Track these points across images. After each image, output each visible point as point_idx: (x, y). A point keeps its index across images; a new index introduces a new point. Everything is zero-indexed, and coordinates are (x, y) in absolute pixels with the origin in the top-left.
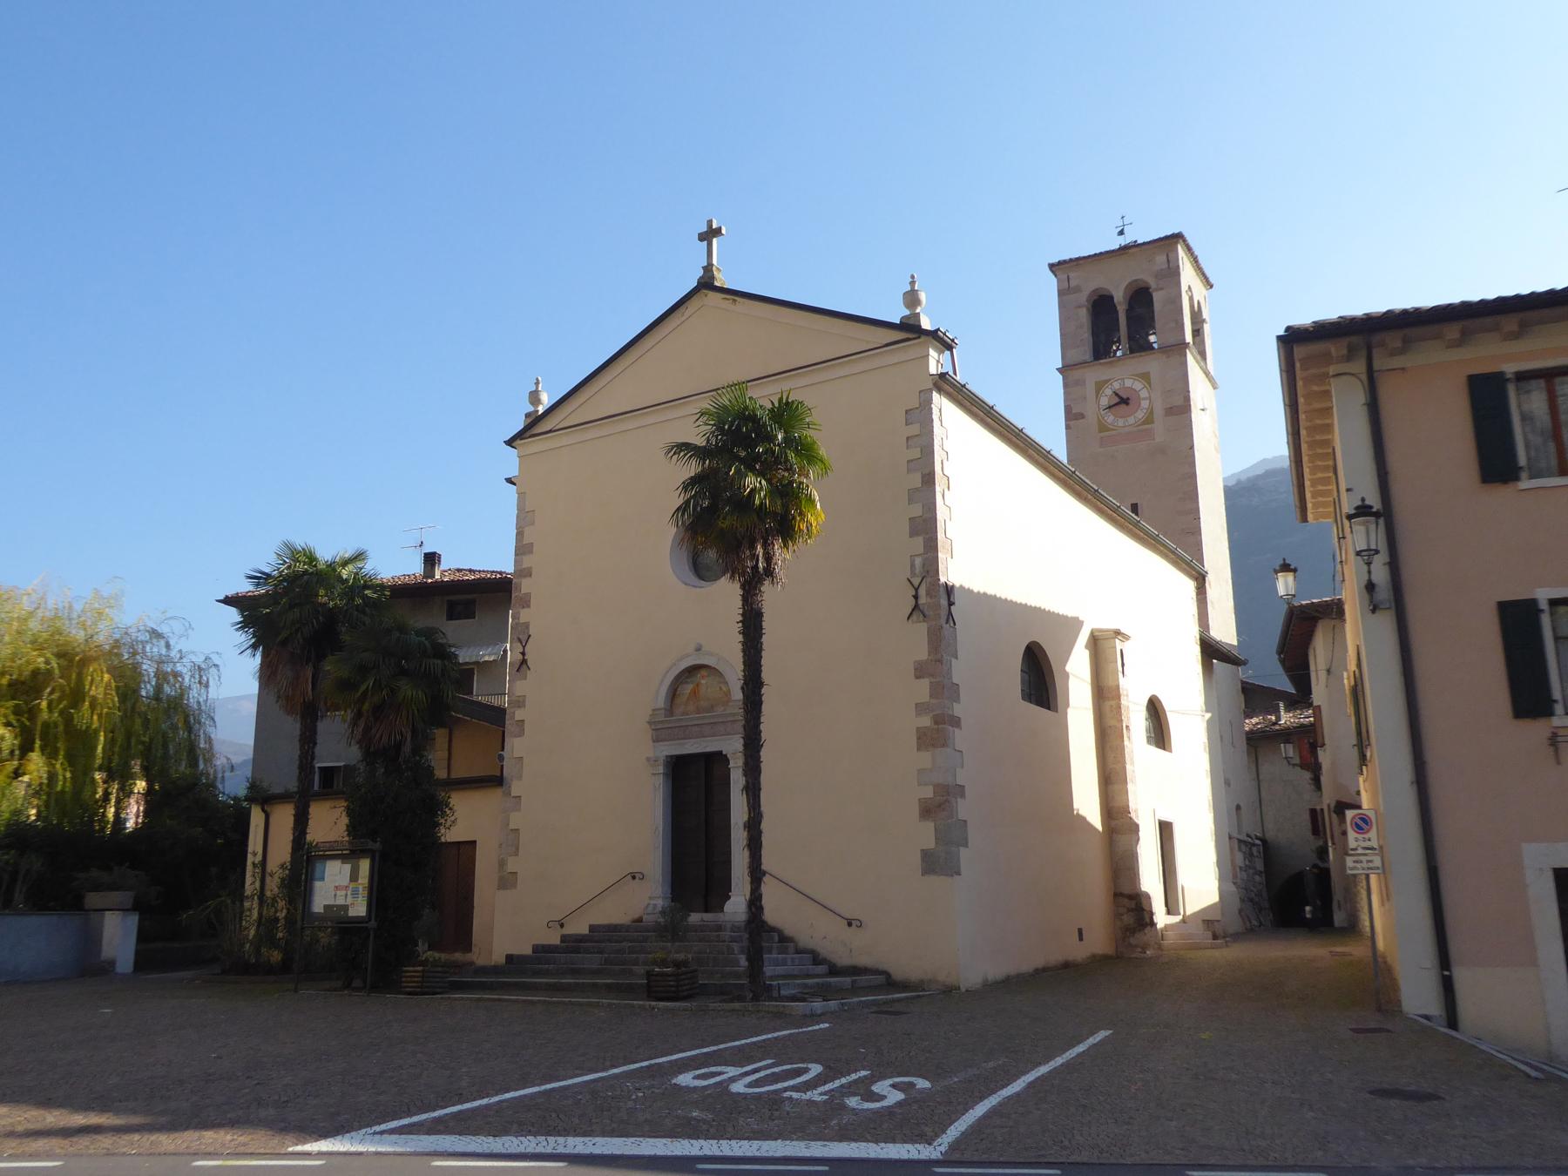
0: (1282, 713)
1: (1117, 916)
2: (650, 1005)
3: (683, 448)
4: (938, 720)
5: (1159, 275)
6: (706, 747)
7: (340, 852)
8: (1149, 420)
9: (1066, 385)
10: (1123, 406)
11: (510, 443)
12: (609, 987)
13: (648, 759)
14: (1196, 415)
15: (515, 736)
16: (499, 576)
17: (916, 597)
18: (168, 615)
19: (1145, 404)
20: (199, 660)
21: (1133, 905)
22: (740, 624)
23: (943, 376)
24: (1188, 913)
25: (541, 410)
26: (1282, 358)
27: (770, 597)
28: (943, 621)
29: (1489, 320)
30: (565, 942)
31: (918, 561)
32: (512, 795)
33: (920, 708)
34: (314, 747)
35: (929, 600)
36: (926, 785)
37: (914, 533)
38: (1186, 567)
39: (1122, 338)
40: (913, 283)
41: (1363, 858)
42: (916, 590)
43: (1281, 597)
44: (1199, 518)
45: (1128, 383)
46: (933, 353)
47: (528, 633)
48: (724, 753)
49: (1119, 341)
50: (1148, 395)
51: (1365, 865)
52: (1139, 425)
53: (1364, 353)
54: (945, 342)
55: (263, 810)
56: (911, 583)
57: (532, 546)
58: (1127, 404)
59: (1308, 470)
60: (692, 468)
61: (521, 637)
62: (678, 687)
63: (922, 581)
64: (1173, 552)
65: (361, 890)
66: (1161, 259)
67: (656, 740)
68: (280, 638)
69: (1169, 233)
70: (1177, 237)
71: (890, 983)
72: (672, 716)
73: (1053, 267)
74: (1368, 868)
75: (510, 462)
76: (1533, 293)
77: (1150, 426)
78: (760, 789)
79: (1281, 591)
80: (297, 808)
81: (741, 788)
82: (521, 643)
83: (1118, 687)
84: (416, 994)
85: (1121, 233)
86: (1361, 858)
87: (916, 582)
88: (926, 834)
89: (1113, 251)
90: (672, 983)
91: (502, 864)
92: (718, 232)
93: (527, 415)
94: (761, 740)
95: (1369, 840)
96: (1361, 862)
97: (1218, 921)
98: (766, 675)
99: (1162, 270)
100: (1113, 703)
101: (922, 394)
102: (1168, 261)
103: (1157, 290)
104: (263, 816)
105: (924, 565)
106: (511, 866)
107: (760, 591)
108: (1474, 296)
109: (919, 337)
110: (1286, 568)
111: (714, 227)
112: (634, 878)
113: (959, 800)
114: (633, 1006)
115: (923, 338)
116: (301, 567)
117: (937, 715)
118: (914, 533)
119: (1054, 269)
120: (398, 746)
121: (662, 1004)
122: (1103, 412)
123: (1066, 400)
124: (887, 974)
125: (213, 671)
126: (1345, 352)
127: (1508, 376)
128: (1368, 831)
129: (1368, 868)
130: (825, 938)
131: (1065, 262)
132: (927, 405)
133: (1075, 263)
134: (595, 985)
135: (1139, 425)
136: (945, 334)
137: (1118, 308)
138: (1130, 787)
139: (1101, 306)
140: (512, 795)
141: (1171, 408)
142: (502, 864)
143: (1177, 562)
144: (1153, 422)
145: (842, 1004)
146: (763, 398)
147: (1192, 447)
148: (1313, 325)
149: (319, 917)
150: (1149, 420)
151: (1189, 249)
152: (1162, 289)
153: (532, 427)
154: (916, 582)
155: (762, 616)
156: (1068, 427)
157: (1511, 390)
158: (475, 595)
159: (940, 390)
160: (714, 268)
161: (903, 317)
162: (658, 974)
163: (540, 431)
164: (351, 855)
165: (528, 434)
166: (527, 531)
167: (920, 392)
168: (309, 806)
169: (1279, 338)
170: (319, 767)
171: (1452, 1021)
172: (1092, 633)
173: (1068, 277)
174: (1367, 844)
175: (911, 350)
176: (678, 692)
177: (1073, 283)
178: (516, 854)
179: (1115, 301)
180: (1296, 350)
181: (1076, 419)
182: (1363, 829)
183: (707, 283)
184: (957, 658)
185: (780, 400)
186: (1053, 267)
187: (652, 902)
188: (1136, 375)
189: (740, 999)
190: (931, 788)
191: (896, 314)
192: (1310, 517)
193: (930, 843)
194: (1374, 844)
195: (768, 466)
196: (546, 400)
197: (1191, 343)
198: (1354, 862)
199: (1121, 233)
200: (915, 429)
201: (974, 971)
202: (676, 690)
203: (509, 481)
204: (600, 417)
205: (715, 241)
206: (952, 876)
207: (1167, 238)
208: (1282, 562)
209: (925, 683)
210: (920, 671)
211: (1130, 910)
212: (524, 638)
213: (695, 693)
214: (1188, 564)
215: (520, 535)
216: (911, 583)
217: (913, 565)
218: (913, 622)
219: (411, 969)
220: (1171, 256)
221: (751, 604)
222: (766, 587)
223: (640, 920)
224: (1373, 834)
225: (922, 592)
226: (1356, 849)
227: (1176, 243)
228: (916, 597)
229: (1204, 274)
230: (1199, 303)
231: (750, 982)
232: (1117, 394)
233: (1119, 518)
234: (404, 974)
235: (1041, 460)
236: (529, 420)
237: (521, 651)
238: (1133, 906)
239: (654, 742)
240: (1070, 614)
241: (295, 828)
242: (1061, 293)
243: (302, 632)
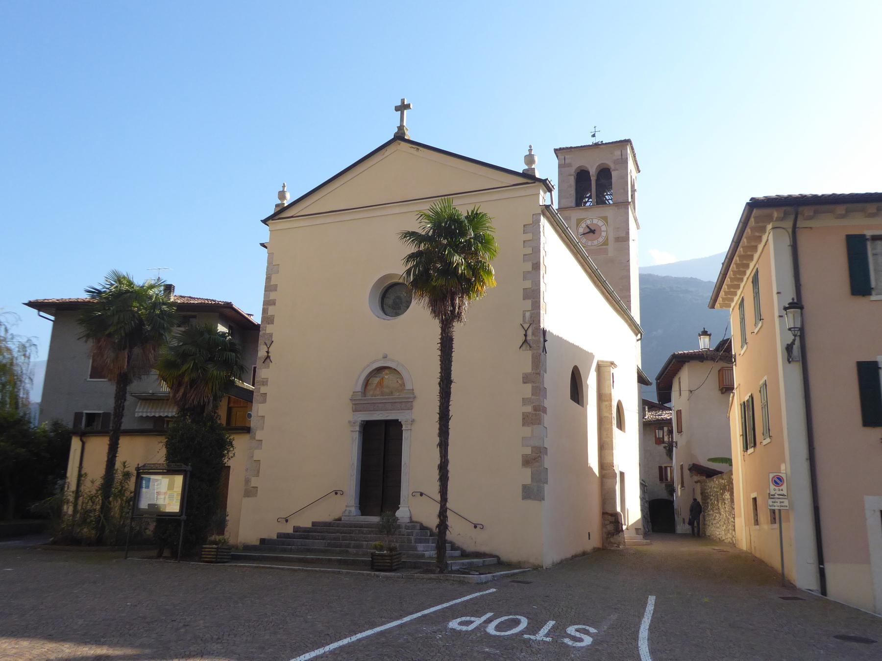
0: (647, 412)
1: (604, 525)
2: (375, 574)
3: (412, 234)
4: (536, 409)
5: (616, 162)
6: (387, 416)
7: (162, 471)
8: (606, 243)
10: (591, 234)
11: (265, 221)
12: (339, 561)
13: (350, 422)
14: (631, 243)
15: (260, 403)
16: (213, 303)
17: (526, 335)
18: (4, 311)
19: (604, 234)
20: (24, 340)
21: (613, 519)
22: (439, 345)
23: (547, 207)
24: (630, 524)
25: (286, 203)
26: (745, 215)
27: (457, 328)
28: (541, 351)
29: (860, 205)
30: (297, 532)
31: (528, 314)
32: (256, 439)
33: (525, 401)
34: (124, 402)
35: (534, 338)
36: (528, 446)
37: (526, 297)
40: (530, 150)
41: (779, 501)
42: (526, 331)
45: (595, 221)
46: (542, 193)
47: (272, 340)
48: (399, 421)
50: (606, 229)
51: (779, 504)
52: (600, 246)
53: (792, 217)
54: (549, 186)
55: (81, 440)
56: (523, 327)
57: (277, 287)
58: (594, 233)
60: (412, 249)
61: (267, 342)
62: (370, 379)
63: (530, 326)
65: (175, 496)
66: (617, 153)
67: (355, 410)
68: (107, 332)
70: (628, 142)
71: (500, 564)
72: (365, 397)
73: (557, 151)
74: (781, 506)
75: (264, 233)
76: (833, 194)
77: (604, 247)
78: (448, 445)
80: (111, 440)
81: (437, 444)
82: (266, 345)
83: (611, 394)
84: (212, 562)
85: (594, 136)
86: (777, 500)
87: (526, 326)
88: (526, 476)
89: (589, 146)
90: (388, 561)
91: (247, 481)
92: (408, 107)
93: (277, 206)
94: (449, 416)
95: (782, 490)
96: (777, 502)
97: (640, 529)
98: (454, 376)
99: (618, 159)
100: (607, 403)
101: (534, 216)
103: (614, 170)
104: (80, 443)
105: (531, 317)
106: (254, 482)
107: (453, 326)
108: (839, 191)
109: (535, 183)
110: (705, 333)
111: (405, 103)
112: (336, 493)
113: (545, 456)
114: (363, 574)
115: (537, 183)
116: (124, 288)
117: (535, 405)
118: (526, 297)
119: (557, 152)
120: (203, 408)
121: (383, 574)
122: (580, 237)
124: (498, 557)
125: (33, 348)
126: (782, 215)
127: (868, 237)
128: (782, 485)
129: (781, 506)
130: (459, 534)
131: (563, 149)
132: (536, 223)
133: (569, 150)
134: (330, 560)
135: (600, 246)
136: (550, 182)
137: (592, 178)
138: (614, 451)
139: (582, 177)
140: (256, 439)
141: (618, 238)
142: (247, 481)
144: (608, 245)
145: (493, 576)
146: (463, 208)
147: (629, 261)
149: (145, 512)
150: (606, 243)
151: (632, 149)
152: (617, 170)
153: (281, 213)
154: (526, 326)
155: (453, 341)
157: (869, 245)
158: (196, 313)
159: (544, 215)
160: (405, 128)
161: (524, 170)
162: (379, 555)
163: (283, 216)
164: (170, 471)
165: (275, 218)
166: (273, 277)
167: (533, 215)
168: (119, 439)
170: (87, 414)
171: (824, 591)
172: (598, 362)
174: (781, 492)
175: (529, 190)
176: (369, 382)
177: (567, 161)
178: (257, 475)
182: (779, 484)
183: (400, 136)
184: (546, 373)
185: (473, 212)
186: (557, 151)
187: (348, 509)
189: (433, 572)
190: (530, 448)
191: (520, 167)
192: (717, 305)
193: (528, 481)
194: (785, 492)
195: (466, 250)
196: (289, 199)
198: (772, 502)
199: (594, 136)
200: (529, 236)
201: (550, 557)
202: (368, 381)
203: (263, 245)
204: (328, 211)
205: (405, 111)
206: (541, 501)
209: (529, 386)
210: (526, 379)
211: (611, 522)
212: (268, 343)
213: (380, 384)
215: (268, 279)
216: (523, 327)
217: (524, 316)
218: (523, 350)
219: (208, 546)
221: (447, 333)
222: (456, 324)
223: (340, 519)
224: (784, 487)
225: (530, 332)
226: (774, 495)
227: (627, 145)
228: (526, 335)
229: (637, 164)
231: (437, 562)
232: (588, 227)
234: (203, 550)
235: (582, 261)
236: (278, 209)
237: (267, 350)
238: (614, 521)
239: (353, 412)
241: (109, 453)
242: (560, 166)
243: (125, 329)
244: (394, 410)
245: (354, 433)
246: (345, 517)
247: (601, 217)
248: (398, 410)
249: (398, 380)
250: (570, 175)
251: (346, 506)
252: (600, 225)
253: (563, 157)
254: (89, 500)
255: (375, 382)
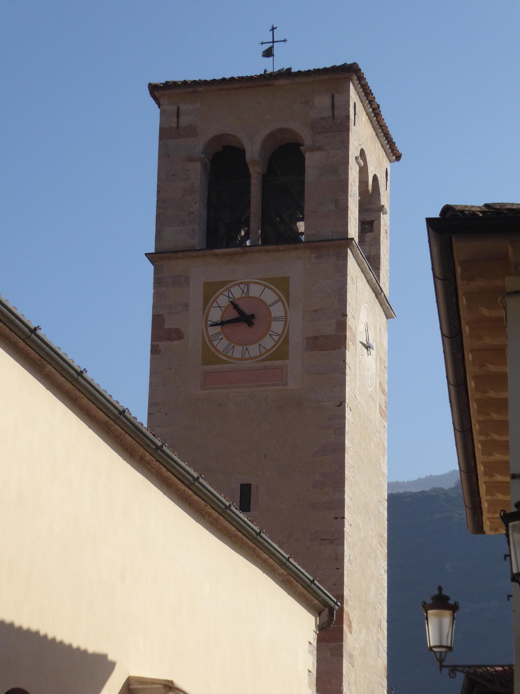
9: (158, 282)
10: (242, 327)
19: (277, 327)
38: (303, 590)
39: (252, 219)
43: (431, 649)
44: (343, 518)
45: (255, 291)
49: (247, 223)
50: (283, 314)
52: (267, 359)
59: (480, 446)
64: (283, 565)
69: (339, 63)
79: (432, 640)
85: (269, 53)
102: (333, 106)
103: (312, 149)
123: (155, 306)
135: (267, 359)
137: (251, 170)
141: (316, 338)
143: (291, 582)
147: (341, 404)
148: (485, 209)
152: (319, 149)
156: (155, 350)
169: (430, 222)
173: (178, 108)
177: (184, 121)
179: (248, 157)
180: (456, 245)
181: (170, 339)
188: (270, 280)
197: (357, 240)
199: (269, 53)
207: (334, 69)
208: (436, 592)
214: (307, 587)
220: (338, 98)
230: (375, 178)
233: (196, 497)
235: (68, 385)
240: (92, 649)
247: (272, 281)
250: (192, 159)
252: (268, 303)
253: (175, 108)
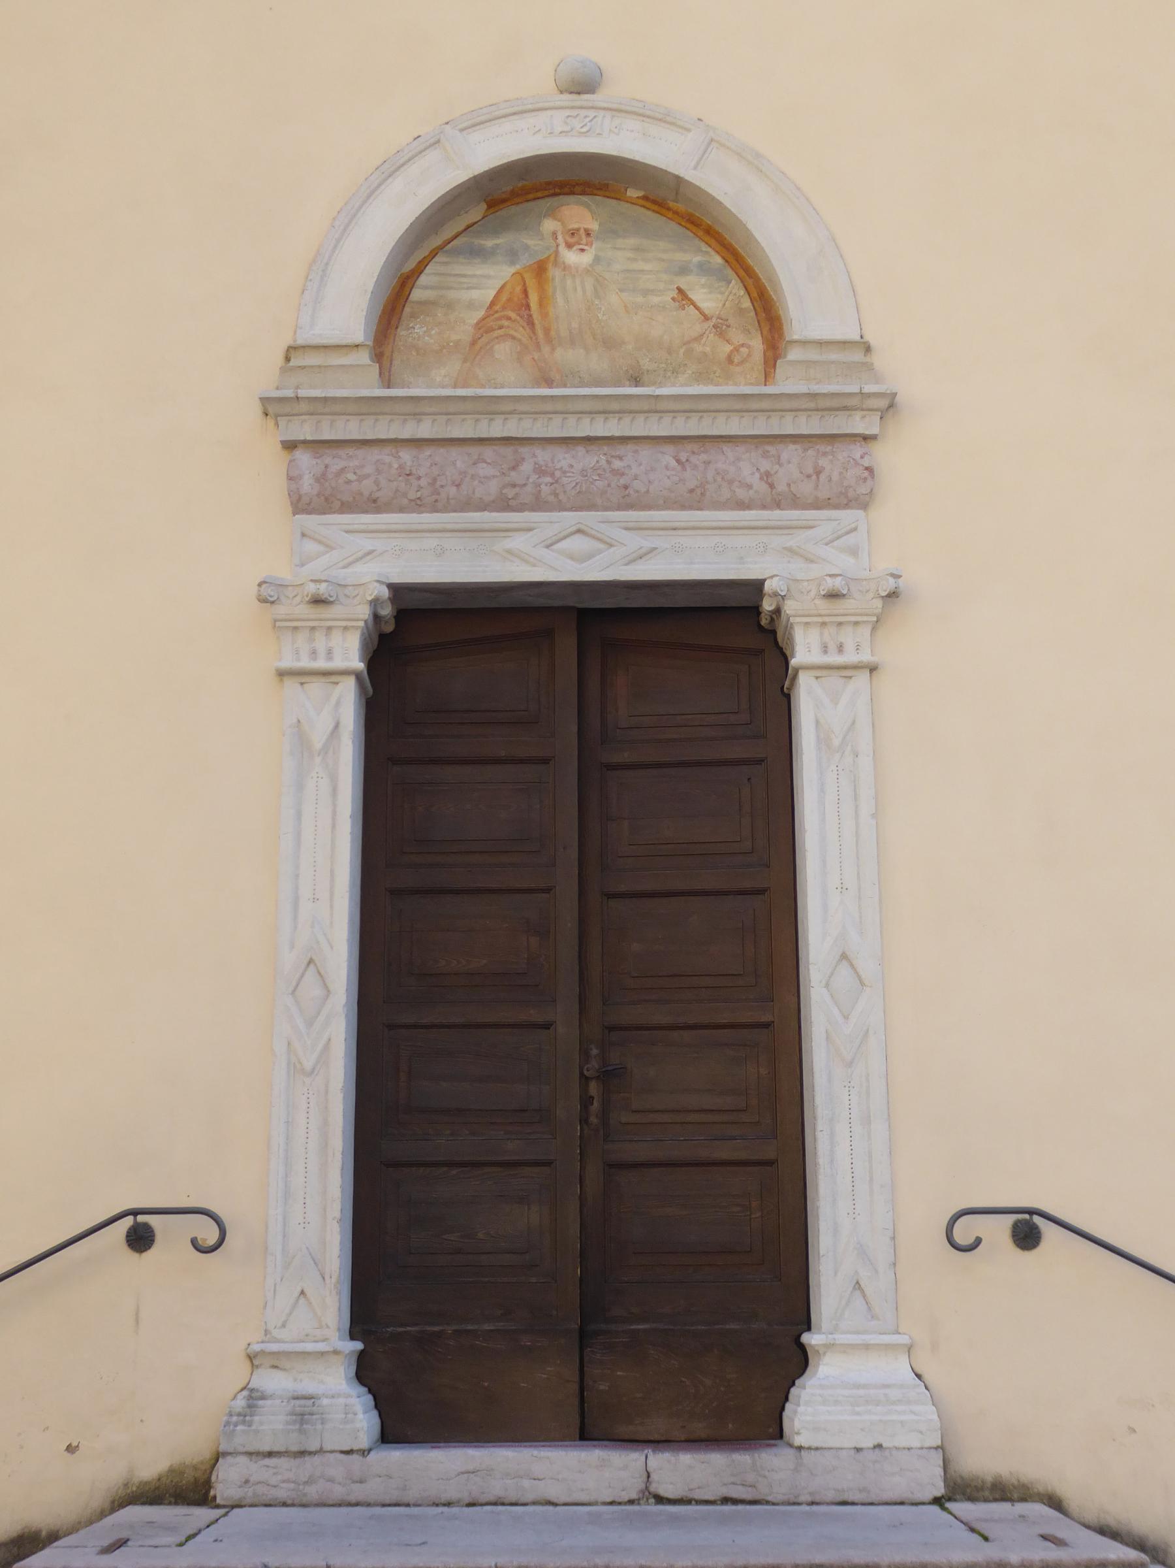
112: (140, 1239)
176: (417, 294)
187: (272, 1381)
244: (696, 500)
245: (316, 687)
246: (258, 1470)
248: (742, 505)
249: (683, 282)
251: (252, 1359)
254: (739, 364)
255: (475, 294)
